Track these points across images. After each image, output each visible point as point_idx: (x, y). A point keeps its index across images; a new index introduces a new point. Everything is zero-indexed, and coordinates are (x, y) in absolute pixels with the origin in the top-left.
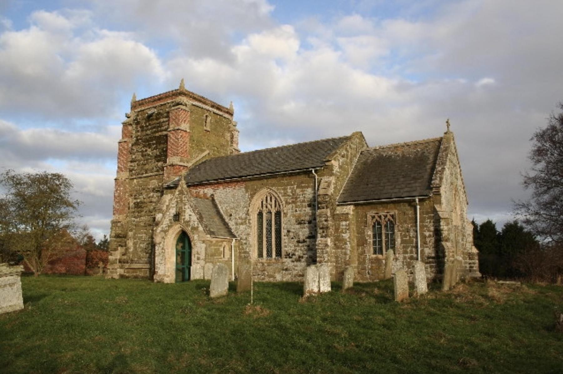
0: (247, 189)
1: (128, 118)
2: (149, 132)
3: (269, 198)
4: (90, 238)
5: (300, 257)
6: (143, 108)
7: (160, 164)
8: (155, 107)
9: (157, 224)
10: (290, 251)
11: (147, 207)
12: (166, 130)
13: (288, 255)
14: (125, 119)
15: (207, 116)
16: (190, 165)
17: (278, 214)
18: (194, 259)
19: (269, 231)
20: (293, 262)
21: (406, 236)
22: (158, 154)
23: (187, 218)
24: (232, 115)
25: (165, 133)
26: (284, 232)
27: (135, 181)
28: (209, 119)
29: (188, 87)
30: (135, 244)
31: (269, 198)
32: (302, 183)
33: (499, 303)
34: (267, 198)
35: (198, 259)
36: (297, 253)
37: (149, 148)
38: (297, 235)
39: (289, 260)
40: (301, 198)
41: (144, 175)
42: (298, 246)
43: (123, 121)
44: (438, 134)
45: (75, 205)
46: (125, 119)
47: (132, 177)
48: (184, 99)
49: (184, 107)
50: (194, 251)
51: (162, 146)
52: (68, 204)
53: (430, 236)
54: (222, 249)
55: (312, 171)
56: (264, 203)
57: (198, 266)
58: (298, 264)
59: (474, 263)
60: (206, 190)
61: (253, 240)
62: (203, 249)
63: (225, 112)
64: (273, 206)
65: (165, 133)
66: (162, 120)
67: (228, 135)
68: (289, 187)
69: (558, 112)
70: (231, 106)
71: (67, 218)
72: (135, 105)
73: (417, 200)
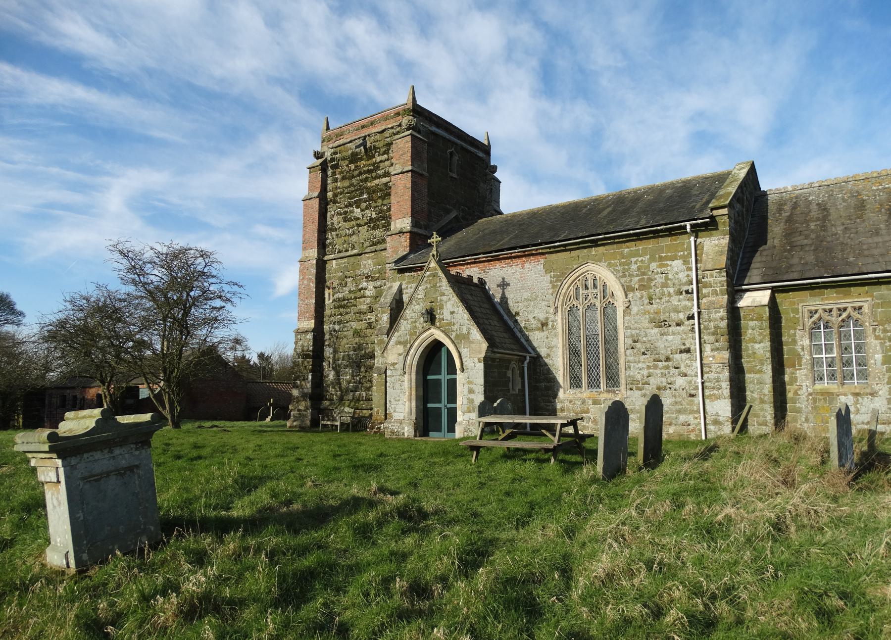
0: (547, 270)
7: (378, 233)
10: (639, 377)
11: (355, 306)
12: (387, 174)
16: (727, 202)
22: (374, 216)
25: (385, 180)
26: (622, 343)
28: (456, 158)
33: (691, 427)
36: (652, 380)
37: (358, 207)
40: (660, 279)
41: (349, 253)
42: (656, 367)
50: (460, 377)
66: (378, 159)
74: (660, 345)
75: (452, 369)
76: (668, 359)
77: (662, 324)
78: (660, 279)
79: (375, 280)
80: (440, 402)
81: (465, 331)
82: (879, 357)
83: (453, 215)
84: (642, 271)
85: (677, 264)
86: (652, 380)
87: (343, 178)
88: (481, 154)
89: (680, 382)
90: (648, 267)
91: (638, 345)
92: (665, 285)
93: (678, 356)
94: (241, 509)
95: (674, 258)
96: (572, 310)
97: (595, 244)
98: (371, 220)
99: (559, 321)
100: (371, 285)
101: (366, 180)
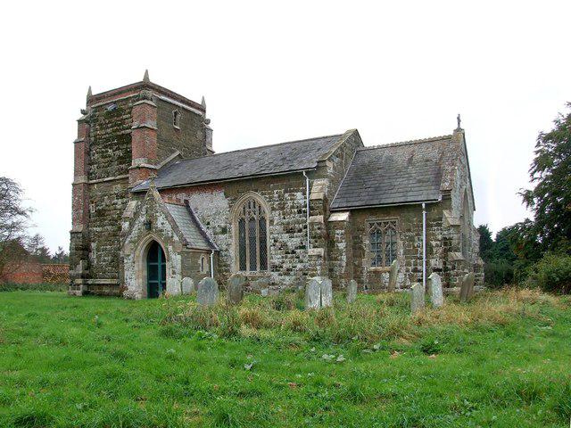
1: (84, 114)
2: (109, 131)
3: (252, 204)
4: (44, 250)
5: (288, 270)
6: (101, 104)
8: (175, 227)
9: (125, 235)
13: (276, 268)
14: (81, 116)
15: (175, 113)
17: (263, 220)
18: (169, 272)
19: (252, 239)
20: (280, 275)
21: (409, 246)
23: (159, 225)
24: (204, 111)
25: (128, 131)
26: (269, 242)
27: (96, 186)
29: (153, 80)
30: (99, 257)
31: (252, 204)
32: (291, 186)
34: (155, 286)
35: (174, 273)
36: (284, 265)
38: (284, 245)
39: (275, 274)
40: (290, 204)
43: (78, 118)
44: (448, 130)
45: (28, 213)
46: (81, 116)
47: (91, 182)
48: (150, 93)
49: (149, 102)
50: (168, 264)
51: (125, 146)
52: (17, 211)
53: (437, 245)
54: (200, 262)
55: (302, 173)
56: (247, 210)
57: (176, 281)
58: (287, 278)
59: (480, 276)
60: (178, 196)
61: (233, 252)
62: (179, 262)
63: (196, 108)
64: (257, 213)
65: (128, 131)
67: (200, 133)
68: (275, 191)
69: (566, 111)
70: (203, 101)
71: (18, 229)
72: (92, 99)
73: (424, 205)
74: (289, 244)
75: (164, 260)
76: (293, 252)
77: (290, 231)
78: (290, 204)
79: (122, 197)
80: (157, 279)
81: (170, 235)
82: (402, 251)
83: (178, 153)
84: (281, 197)
85: (299, 195)
86: (284, 265)
87: (101, 129)
88: (201, 113)
89: (299, 266)
90: (283, 196)
91: (277, 244)
92: (292, 207)
93: (298, 251)
94: (14, 366)
95: (297, 191)
96: (242, 222)
97: (443, 139)
98: (119, 157)
99: (234, 228)
100: (120, 201)
101: (117, 130)
